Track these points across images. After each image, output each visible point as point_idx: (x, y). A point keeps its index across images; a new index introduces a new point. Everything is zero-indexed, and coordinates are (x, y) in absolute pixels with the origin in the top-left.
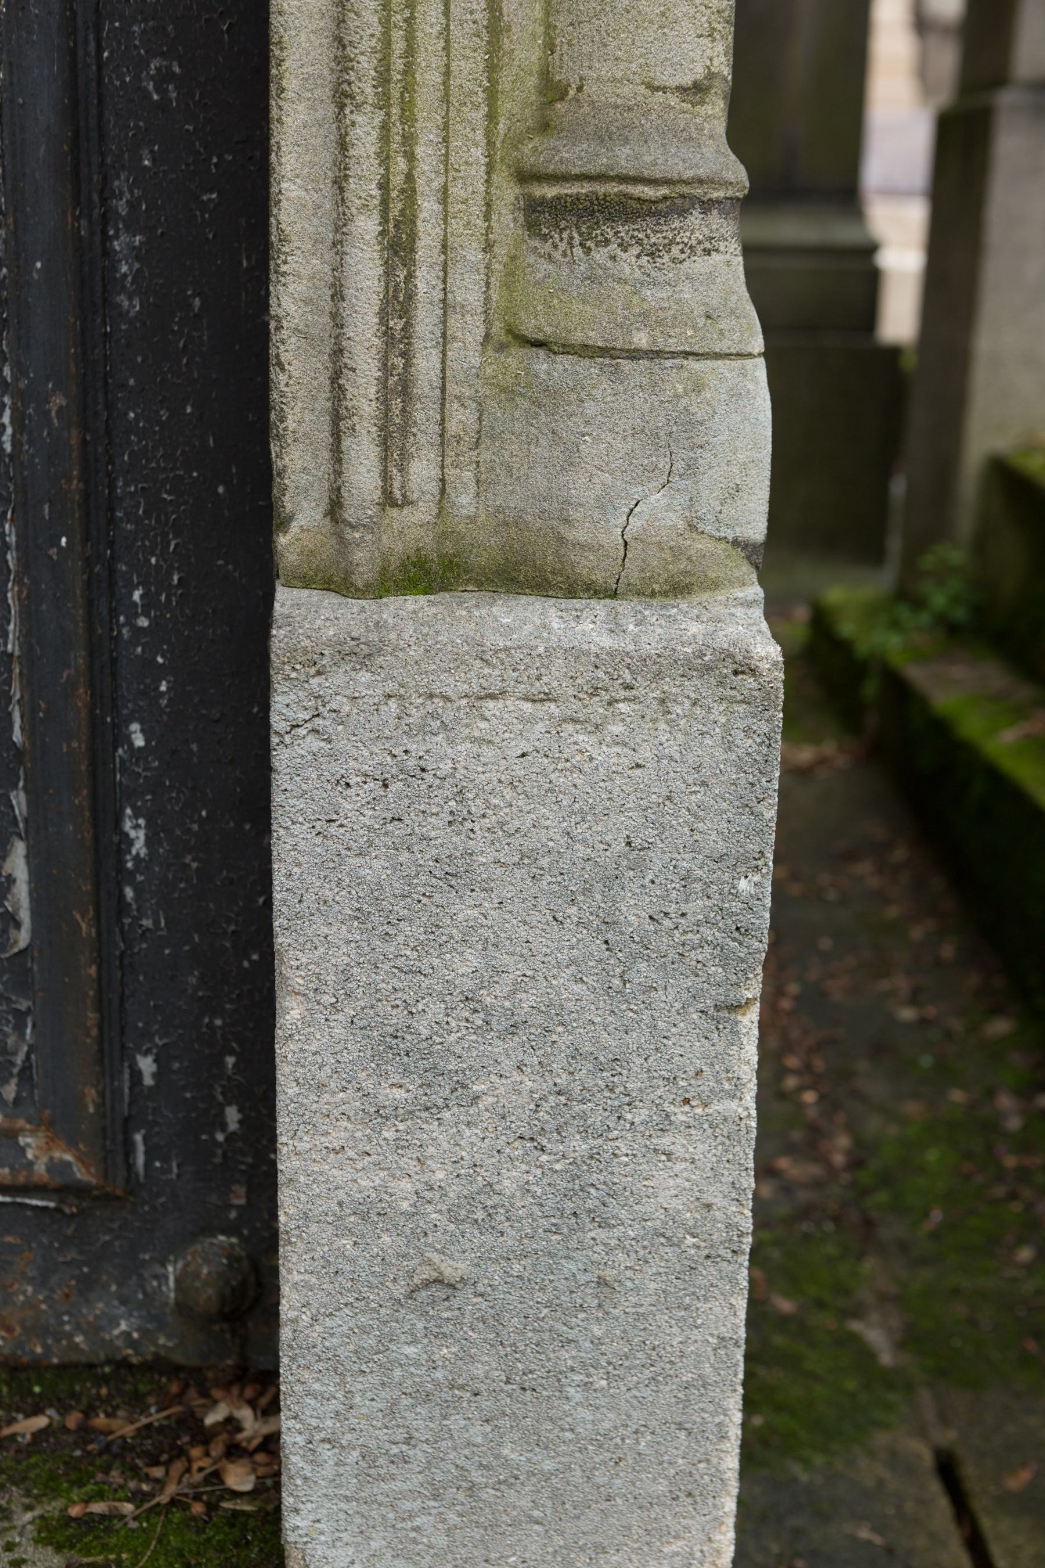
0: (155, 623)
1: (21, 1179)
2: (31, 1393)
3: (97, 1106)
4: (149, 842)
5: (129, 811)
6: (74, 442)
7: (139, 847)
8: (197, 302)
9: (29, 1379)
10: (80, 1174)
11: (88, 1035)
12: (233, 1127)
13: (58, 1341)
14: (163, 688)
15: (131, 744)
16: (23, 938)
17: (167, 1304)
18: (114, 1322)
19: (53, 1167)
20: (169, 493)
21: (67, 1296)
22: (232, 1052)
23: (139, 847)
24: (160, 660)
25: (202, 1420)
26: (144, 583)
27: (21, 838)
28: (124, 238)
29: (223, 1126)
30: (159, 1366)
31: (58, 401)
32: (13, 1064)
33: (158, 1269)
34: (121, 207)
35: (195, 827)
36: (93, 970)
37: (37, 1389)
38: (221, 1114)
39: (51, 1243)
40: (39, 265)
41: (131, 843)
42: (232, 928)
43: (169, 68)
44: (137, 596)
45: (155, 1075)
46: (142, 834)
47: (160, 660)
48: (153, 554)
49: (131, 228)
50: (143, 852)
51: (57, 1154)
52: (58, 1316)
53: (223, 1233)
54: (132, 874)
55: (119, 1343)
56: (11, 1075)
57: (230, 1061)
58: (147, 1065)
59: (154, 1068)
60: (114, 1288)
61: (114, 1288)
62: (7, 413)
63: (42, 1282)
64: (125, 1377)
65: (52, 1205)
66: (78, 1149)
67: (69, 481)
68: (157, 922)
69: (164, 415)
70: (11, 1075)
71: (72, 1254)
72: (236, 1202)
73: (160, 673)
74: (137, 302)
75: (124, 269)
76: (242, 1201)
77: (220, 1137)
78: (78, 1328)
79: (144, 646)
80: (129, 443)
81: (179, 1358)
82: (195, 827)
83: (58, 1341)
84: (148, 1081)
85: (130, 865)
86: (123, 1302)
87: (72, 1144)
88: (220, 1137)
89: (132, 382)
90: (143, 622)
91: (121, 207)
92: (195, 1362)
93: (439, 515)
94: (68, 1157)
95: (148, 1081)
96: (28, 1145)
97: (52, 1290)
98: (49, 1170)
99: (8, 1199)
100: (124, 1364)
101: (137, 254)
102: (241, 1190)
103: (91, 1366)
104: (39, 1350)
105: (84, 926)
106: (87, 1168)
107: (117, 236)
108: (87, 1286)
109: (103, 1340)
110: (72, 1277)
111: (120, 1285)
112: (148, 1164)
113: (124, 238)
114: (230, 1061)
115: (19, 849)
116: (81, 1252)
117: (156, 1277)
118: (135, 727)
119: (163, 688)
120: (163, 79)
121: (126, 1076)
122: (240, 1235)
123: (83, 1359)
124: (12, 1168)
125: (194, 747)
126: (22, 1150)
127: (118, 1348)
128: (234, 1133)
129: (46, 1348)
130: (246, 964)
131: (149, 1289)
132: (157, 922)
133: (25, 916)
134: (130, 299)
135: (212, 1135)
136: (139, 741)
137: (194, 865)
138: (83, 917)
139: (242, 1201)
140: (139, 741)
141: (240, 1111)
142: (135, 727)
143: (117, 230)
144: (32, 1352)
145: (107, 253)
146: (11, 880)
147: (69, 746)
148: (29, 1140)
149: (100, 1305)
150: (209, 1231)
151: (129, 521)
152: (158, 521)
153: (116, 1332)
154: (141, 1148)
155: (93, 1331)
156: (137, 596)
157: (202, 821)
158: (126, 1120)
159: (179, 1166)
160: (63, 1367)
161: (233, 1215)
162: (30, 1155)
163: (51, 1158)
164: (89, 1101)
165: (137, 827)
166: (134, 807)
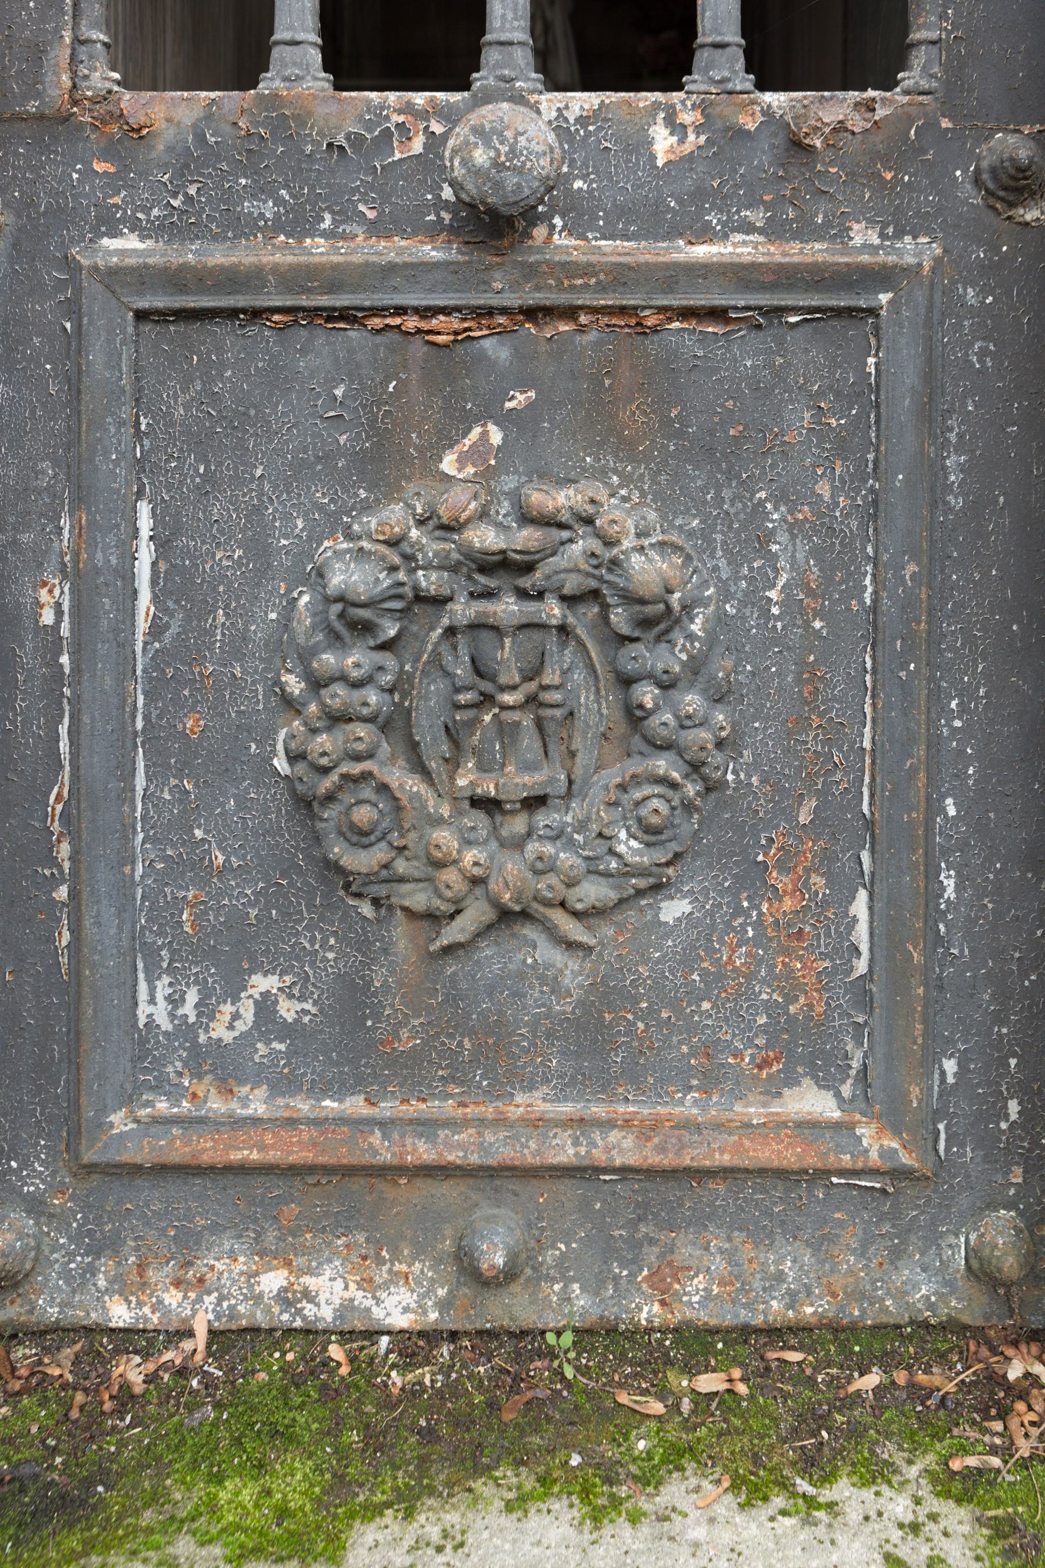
0: (967, 724)
1: (860, 1165)
2: (852, 1352)
3: (920, 1101)
4: (958, 888)
5: (943, 865)
6: (923, 596)
7: (950, 893)
8: (1002, 499)
9: (848, 1340)
10: (906, 1159)
11: (915, 1043)
12: (1014, 1117)
13: (872, 1304)
14: (971, 772)
15: (946, 814)
16: (861, 966)
17: (958, 1271)
18: (916, 1287)
19: (883, 1153)
20: (978, 630)
21: (881, 1264)
22: (1014, 1055)
23: (950, 893)
24: (969, 751)
25: (1004, 1376)
26: (960, 696)
27: (865, 887)
28: (953, 458)
29: (1007, 1116)
30: (952, 1326)
31: (912, 568)
32: (850, 1067)
33: (952, 1240)
34: (953, 437)
35: (991, 876)
36: (921, 991)
37: (857, 1349)
38: (1006, 1107)
39: (871, 1218)
40: (901, 477)
41: (944, 889)
42: (1017, 955)
43: (987, 347)
44: (953, 705)
45: (955, 1075)
46: (952, 882)
47: (969, 751)
48: (966, 674)
49: (958, 452)
50: (953, 896)
51: (886, 1143)
52: (873, 1282)
53: (1004, 1208)
54: (944, 913)
55: (920, 1306)
56: (848, 1076)
57: (1013, 1062)
58: (950, 1066)
59: (955, 1069)
60: (917, 1257)
61: (917, 1257)
62: (869, 578)
63: (862, 1252)
64: (929, 1337)
65: (878, 1185)
66: (901, 1138)
67: (919, 623)
68: (962, 951)
69: (977, 576)
70: (848, 1076)
71: (886, 1228)
72: (1014, 1181)
73: (968, 761)
74: (960, 500)
75: (953, 478)
76: (1020, 1180)
77: (1004, 1126)
78: (888, 1293)
79: (958, 741)
80: (952, 597)
81: (966, 1319)
82: (991, 876)
83: (872, 1304)
84: (950, 1080)
85: (943, 906)
86: (924, 1270)
87: (897, 1133)
88: (1004, 1126)
89: (955, 554)
90: (957, 723)
91: (953, 437)
92: (980, 1322)
93: (441, 666)
94: (895, 1145)
95: (950, 1080)
96: (863, 1135)
97: (870, 1260)
98: (881, 1156)
99: (843, 1181)
100: (926, 1325)
101: (962, 468)
102: (1018, 1170)
103: (898, 1327)
104: (857, 1313)
105: (915, 955)
106: (910, 1153)
107: (948, 457)
108: (897, 1255)
109: (907, 1303)
110: (886, 1248)
111: (922, 1254)
112: (947, 1150)
113: (953, 458)
114: (1013, 1062)
115: (862, 895)
116: (893, 1226)
117: (950, 1246)
118: (949, 801)
119: (971, 772)
120: (983, 354)
121: (936, 1076)
122: (1017, 1209)
123: (892, 1321)
124: (853, 1156)
125: (992, 815)
126: (859, 1139)
127: (920, 1311)
128: (1015, 1122)
129: (863, 1311)
130: (1027, 983)
131: (945, 1258)
132: (962, 951)
133: (864, 948)
134: (956, 498)
135: (998, 1125)
136: (952, 811)
137: (990, 906)
138: (915, 948)
139: (1020, 1180)
140: (952, 811)
141: (1019, 1104)
142: (949, 801)
143: (949, 452)
144: (852, 1314)
145: (944, 468)
146: (855, 920)
147: (909, 816)
148: (863, 1131)
149: (907, 1272)
150: (992, 1205)
151: (950, 651)
152: (970, 651)
153: (918, 1296)
154: (943, 1136)
155: (900, 1295)
156: (953, 705)
157: (997, 872)
158: (936, 1112)
159: (972, 1150)
160: (874, 1327)
161: (1012, 1192)
162: (865, 1142)
163: (882, 1146)
164: (913, 1096)
165: (949, 877)
166: (947, 862)
